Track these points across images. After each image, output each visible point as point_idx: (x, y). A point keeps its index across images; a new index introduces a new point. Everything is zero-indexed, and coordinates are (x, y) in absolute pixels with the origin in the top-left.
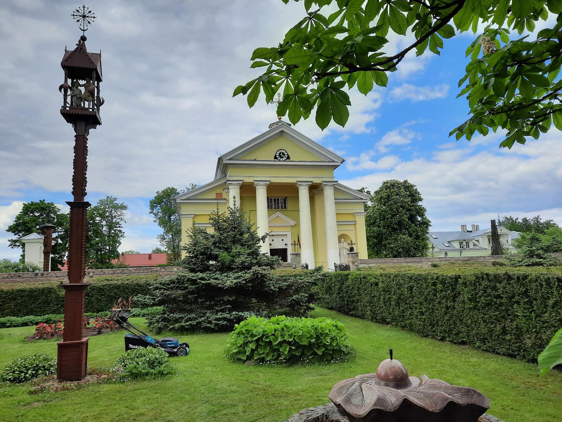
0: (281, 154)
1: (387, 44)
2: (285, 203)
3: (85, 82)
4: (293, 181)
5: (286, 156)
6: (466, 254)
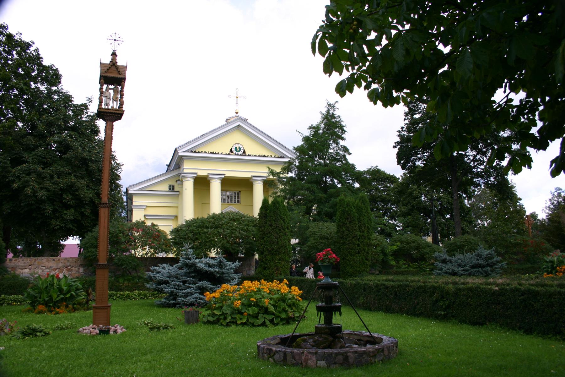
0: (238, 150)
1: (103, 62)
2: (238, 198)
3: (114, 87)
4: (248, 175)
5: (243, 151)
6: (399, 270)
